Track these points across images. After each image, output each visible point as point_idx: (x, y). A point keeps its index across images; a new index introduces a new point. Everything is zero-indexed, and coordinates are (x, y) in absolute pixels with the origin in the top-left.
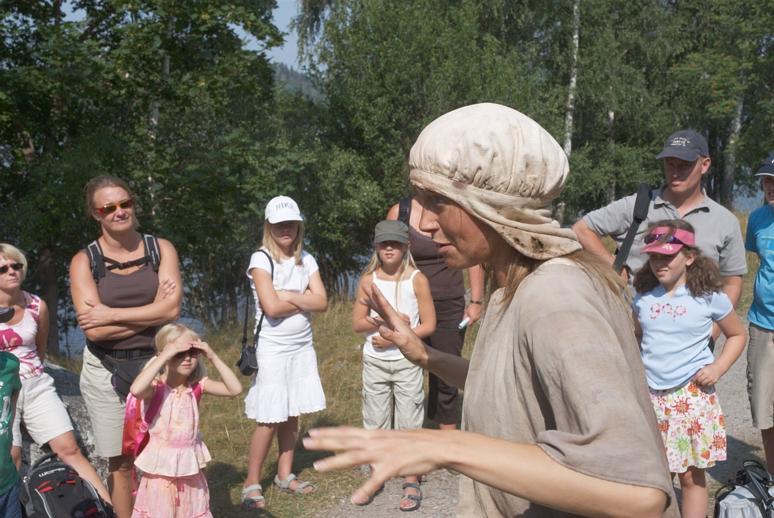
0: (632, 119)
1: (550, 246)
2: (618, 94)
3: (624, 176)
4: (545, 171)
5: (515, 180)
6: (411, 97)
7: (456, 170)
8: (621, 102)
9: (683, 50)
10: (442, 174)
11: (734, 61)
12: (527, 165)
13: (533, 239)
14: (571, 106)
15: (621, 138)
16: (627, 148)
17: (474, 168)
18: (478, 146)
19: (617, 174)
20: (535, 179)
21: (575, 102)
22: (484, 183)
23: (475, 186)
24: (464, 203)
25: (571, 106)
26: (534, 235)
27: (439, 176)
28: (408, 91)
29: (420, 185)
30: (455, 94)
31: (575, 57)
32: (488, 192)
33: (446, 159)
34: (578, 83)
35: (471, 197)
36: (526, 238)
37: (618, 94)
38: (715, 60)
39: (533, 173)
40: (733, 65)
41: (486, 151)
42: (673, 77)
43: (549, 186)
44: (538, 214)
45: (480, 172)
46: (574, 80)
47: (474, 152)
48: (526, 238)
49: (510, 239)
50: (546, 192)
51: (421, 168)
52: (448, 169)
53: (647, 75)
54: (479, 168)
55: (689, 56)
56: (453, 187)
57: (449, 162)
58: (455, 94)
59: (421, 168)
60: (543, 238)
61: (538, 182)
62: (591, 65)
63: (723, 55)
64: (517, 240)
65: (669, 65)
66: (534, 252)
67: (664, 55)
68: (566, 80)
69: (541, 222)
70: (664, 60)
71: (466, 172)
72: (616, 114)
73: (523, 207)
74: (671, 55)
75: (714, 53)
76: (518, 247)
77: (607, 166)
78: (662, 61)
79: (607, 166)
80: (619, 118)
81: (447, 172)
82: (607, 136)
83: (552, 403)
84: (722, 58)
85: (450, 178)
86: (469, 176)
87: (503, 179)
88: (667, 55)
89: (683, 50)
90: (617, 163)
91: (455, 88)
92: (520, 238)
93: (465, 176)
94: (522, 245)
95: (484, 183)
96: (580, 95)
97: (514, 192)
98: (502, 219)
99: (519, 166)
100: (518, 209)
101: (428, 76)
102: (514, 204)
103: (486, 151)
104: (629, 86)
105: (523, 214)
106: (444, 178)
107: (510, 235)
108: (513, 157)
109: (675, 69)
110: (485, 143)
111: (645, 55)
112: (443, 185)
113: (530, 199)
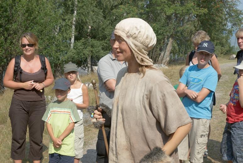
0: (98, 29)
1: (145, 62)
2: (93, 19)
3: (95, 52)
4: (151, 41)
5: (143, 40)
6: (7, 14)
7: (128, 32)
8: (93, 23)
9: (117, 4)
10: (125, 32)
11: (137, 9)
12: (147, 37)
13: (142, 59)
14: (74, 23)
15: (94, 37)
16: (96, 41)
17: (134, 33)
18: (136, 27)
19: (92, 51)
20: (148, 42)
21: (76, 21)
22: (135, 38)
23: (132, 38)
24: (128, 42)
25: (74, 23)
26: (142, 57)
27: (123, 33)
28: (6, 11)
29: (117, 34)
30: (27, 14)
31: (76, 3)
32: (135, 41)
33: (127, 29)
34: (77, 14)
35: (130, 41)
36: (140, 57)
37: (93, 19)
38: (130, 8)
39: (148, 40)
40: (136, 10)
41: (138, 30)
42: (113, 14)
43: (150, 45)
44: (145, 52)
45: (135, 35)
46: (75, 12)
47: (135, 29)
48: (140, 57)
49: (136, 57)
50: (149, 47)
51: (119, 30)
52: (126, 31)
53: (104, 12)
54: (135, 34)
55: (120, 6)
56: (126, 37)
57: (128, 30)
58: (27, 14)
59: (119, 30)
60: (144, 59)
61: (148, 43)
62: (83, 6)
63: (133, 6)
64: (137, 57)
65: (112, 9)
66: (141, 62)
67: (110, 4)
68: (72, 12)
69: (145, 55)
70: (110, 7)
71: (131, 33)
72: (92, 27)
73: (142, 48)
74: (113, 5)
75: (129, 6)
76: (137, 59)
77: (89, 48)
78: (109, 7)
79: (89, 48)
80: (93, 29)
81: (126, 32)
82: (88, 36)
83: (216, 102)
84: (132, 8)
85: (126, 34)
86: (132, 35)
87: (140, 39)
88: (111, 5)
89: (117, 4)
90: (92, 47)
91: (27, 11)
92: (138, 57)
93: (130, 35)
94: (138, 59)
95: (135, 38)
96: (79, 18)
97: (142, 43)
98: (136, 50)
99: (145, 37)
100: (141, 48)
101: (15, 6)
102: (140, 46)
103: (138, 30)
104: (97, 16)
105: (142, 50)
106: (124, 34)
107: (136, 55)
108: (144, 34)
109: (114, 11)
110: (138, 28)
111: (103, 4)
112: (124, 36)
113: (145, 47)
